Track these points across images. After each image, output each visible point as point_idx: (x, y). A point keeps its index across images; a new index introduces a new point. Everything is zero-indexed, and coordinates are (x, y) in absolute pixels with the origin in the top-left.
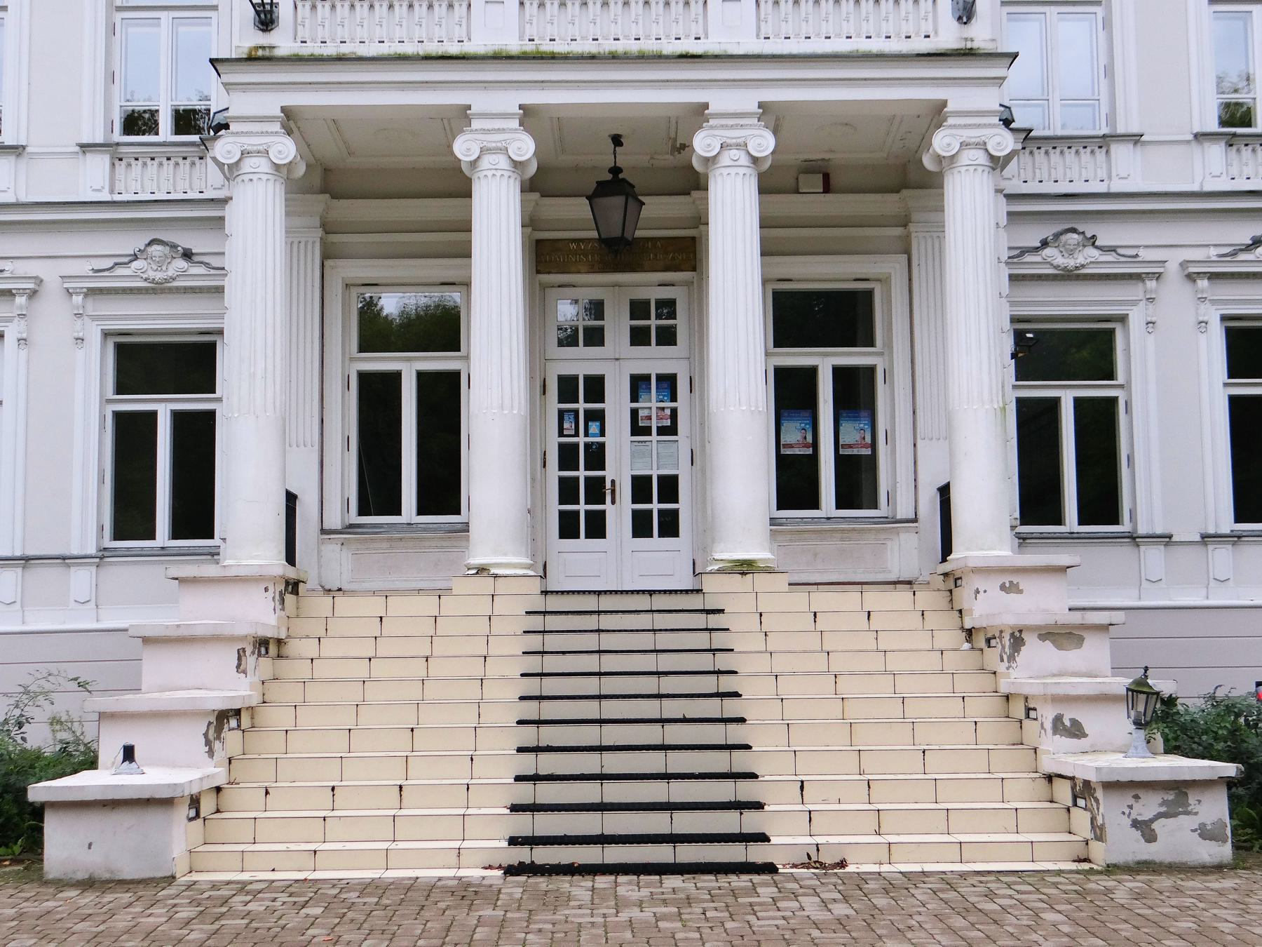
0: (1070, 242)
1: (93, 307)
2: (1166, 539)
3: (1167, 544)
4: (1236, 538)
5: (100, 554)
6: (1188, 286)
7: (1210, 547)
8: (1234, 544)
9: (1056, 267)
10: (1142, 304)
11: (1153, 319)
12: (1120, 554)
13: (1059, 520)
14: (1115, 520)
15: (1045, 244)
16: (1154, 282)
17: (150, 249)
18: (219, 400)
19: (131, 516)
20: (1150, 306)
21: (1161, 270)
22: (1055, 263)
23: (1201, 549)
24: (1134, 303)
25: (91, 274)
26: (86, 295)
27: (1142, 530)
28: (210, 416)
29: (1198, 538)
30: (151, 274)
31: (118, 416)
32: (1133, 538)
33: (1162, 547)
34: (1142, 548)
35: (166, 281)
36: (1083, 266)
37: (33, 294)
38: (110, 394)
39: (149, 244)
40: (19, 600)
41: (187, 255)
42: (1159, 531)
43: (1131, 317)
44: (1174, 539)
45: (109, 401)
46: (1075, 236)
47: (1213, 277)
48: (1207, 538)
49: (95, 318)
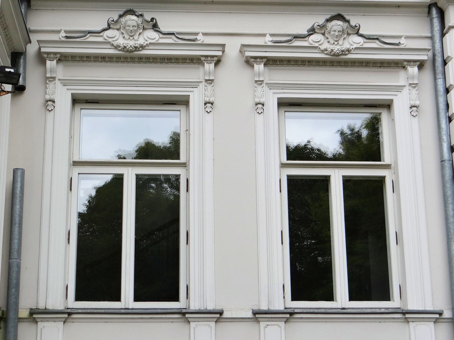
0: (129, 23)
2: (218, 315)
4: (290, 315)
6: (246, 73)
7: (263, 324)
8: (287, 321)
9: (116, 47)
10: (202, 86)
11: (211, 100)
13: (330, 297)
14: (386, 297)
15: (312, 31)
17: (330, 25)
18: (388, 167)
19: (309, 280)
20: (209, 87)
21: (220, 53)
22: (115, 43)
24: (194, 85)
25: (64, 39)
26: (59, 61)
27: (194, 306)
28: (379, 182)
29: (250, 315)
30: (121, 42)
31: (291, 180)
32: (405, 315)
33: (282, 324)
34: (193, 324)
35: (136, 49)
36: (143, 47)
37: (218, 62)
39: (328, 21)
41: (155, 27)
42: (210, 307)
43: (394, 101)
44: (225, 315)
45: (283, 165)
47: (270, 62)
48: (258, 315)
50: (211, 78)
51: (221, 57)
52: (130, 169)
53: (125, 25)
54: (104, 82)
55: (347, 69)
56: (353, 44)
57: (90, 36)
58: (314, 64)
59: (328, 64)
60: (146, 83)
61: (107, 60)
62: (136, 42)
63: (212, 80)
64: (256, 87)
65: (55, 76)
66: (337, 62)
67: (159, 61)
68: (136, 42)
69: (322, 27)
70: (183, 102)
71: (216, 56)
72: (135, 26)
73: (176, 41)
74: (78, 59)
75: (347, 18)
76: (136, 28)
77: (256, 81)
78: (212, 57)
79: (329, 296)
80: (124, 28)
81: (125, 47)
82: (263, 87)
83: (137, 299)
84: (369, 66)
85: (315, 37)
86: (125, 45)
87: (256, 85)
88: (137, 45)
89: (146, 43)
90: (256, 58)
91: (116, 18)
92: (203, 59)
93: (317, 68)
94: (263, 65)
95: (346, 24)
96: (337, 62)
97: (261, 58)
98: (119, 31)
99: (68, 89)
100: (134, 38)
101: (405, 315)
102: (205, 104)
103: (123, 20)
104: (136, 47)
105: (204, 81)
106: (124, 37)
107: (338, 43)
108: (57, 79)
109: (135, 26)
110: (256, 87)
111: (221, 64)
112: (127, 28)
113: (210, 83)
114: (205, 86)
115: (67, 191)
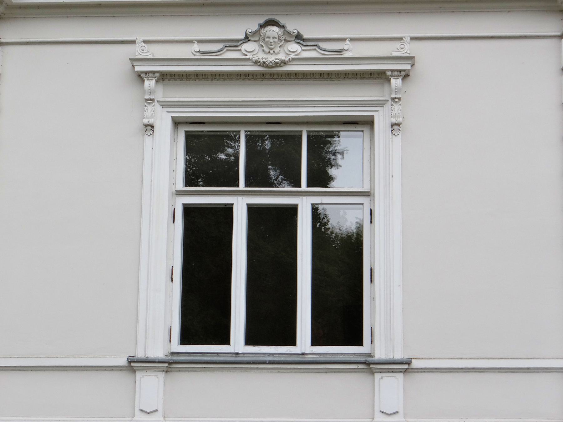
0: (268, 34)
1: (161, 93)
3: (405, 371)
4: (171, 364)
5: (170, 358)
9: (256, 63)
12: (348, 383)
16: (399, 81)
19: (203, 318)
20: (396, 107)
21: (408, 67)
22: (255, 58)
23: (124, 378)
24: (381, 103)
27: (379, 355)
30: (260, 56)
31: (188, 210)
32: (369, 365)
35: (277, 65)
36: (284, 63)
37: (405, 75)
38: (180, 185)
39: (262, 26)
40: (160, 409)
41: (299, 38)
42: (398, 356)
44: (416, 364)
45: (179, 193)
46: (275, 28)
49: (165, 104)
50: (398, 97)
51: (409, 70)
52: (240, 198)
54: (331, 103)
55: (264, 82)
56: (289, 53)
57: (227, 50)
58: (367, 76)
59: (234, 78)
60: (218, 103)
63: (399, 99)
64: (146, 106)
66: (271, 75)
69: (254, 33)
70: (369, 123)
71: (404, 70)
72: (276, 38)
75: (282, 21)
76: (276, 40)
77: (146, 100)
78: (399, 71)
79: (291, 340)
80: (264, 40)
81: (264, 63)
82: (154, 106)
83: (315, 342)
84: (256, 79)
85: (247, 47)
86: (264, 60)
87: (146, 104)
88: (277, 61)
89: (289, 57)
90: (147, 73)
91: (255, 27)
92: (389, 73)
93: (312, 82)
94: (154, 81)
95: (282, 30)
96: (271, 75)
97: (153, 72)
101: (369, 365)
102: (392, 126)
103: (262, 31)
105: (390, 100)
109: (276, 38)
111: (408, 79)
112: (267, 40)
114: (392, 105)
115: (168, 224)
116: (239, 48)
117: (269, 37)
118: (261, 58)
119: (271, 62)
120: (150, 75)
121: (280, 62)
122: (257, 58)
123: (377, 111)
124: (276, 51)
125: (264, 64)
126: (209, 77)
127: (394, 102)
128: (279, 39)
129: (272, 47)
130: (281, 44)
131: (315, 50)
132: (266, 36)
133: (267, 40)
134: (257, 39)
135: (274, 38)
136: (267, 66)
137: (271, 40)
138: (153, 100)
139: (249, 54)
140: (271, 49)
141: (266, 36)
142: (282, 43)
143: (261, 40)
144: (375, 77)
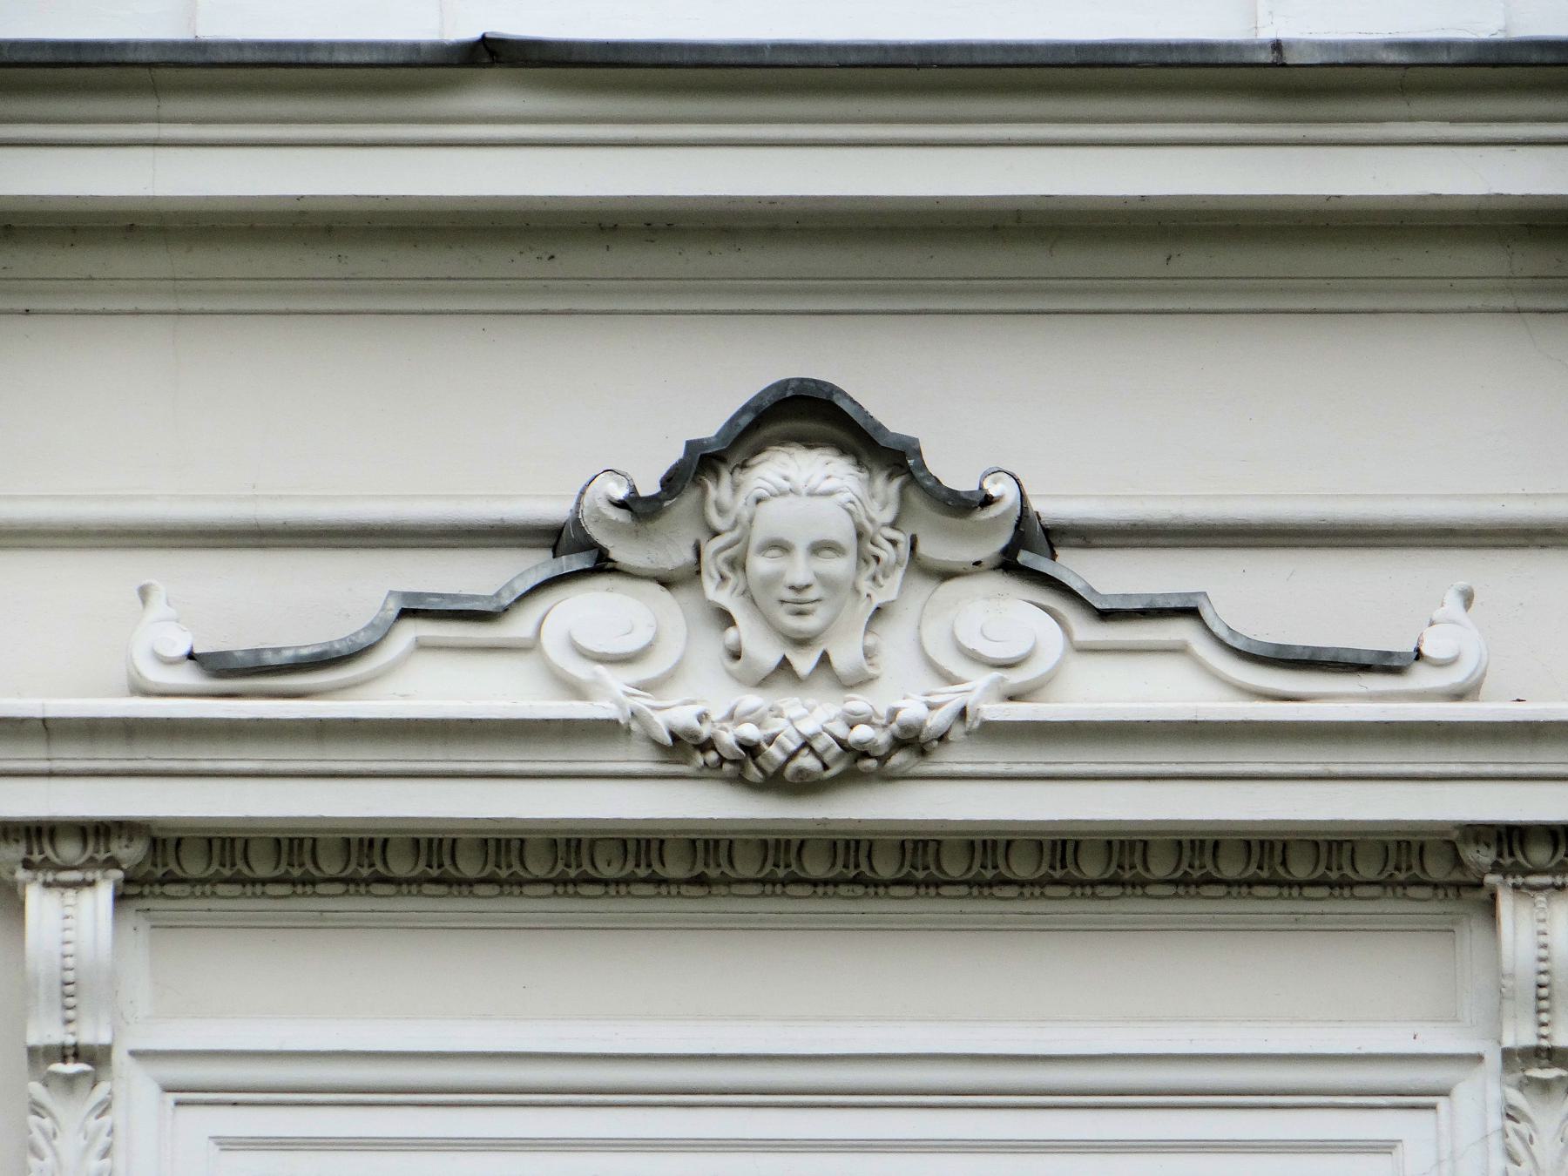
0: (774, 519)
9: (684, 748)
22: (675, 712)
35: (857, 765)
41: (1030, 550)
53: (743, 541)
56: (958, 667)
57: (422, 646)
61: (1092, 869)
62: (859, 702)
64: (37, 1108)
65: (104, 1038)
67: (746, 869)
68: (859, 702)
73: (576, 690)
74: (816, 868)
76: (837, 567)
77: (40, 1056)
80: (738, 564)
81: (751, 750)
82: (105, 1107)
86: (750, 732)
87: (36, 1089)
88: (862, 733)
94: (104, 893)
98: (685, 595)
99: (228, 1144)
100: (825, 659)
104: (855, 753)
105: (1494, 1059)
106: (736, 655)
107: (825, 659)
108: (119, 1057)
110: (37, 1108)
113: (70, 1080)
114: (1511, 1114)
116: (518, 627)
117: (781, 547)
118: (717, 714)
119: (807, 744)
120: (69, 850)
121: (882, 738)
122: (684, 717)
123: (1386, 1147)
124: (845, 657)
125: (746, 765)
126: (746, 868)
127: (1526, 1084)
128: (863, 559)
129: (809, 624)
130: (877, 600)
131: (1178, 650)
132: (758, 536)
133: (761, 565)
134: (676, 556)
135: (820, 548)
136: (778, 782)
137: (800, 569)
138: (95, 1057)
139: (617, 681)
140: (801, 642)
141: (758, 536)
142: (889, 590)
143: (712, 565)
144: (331, 868)
